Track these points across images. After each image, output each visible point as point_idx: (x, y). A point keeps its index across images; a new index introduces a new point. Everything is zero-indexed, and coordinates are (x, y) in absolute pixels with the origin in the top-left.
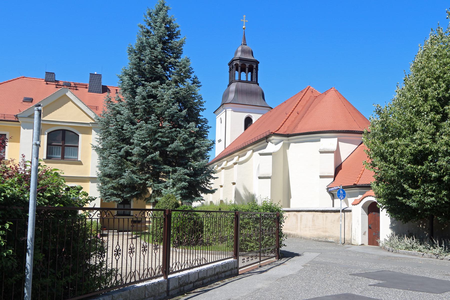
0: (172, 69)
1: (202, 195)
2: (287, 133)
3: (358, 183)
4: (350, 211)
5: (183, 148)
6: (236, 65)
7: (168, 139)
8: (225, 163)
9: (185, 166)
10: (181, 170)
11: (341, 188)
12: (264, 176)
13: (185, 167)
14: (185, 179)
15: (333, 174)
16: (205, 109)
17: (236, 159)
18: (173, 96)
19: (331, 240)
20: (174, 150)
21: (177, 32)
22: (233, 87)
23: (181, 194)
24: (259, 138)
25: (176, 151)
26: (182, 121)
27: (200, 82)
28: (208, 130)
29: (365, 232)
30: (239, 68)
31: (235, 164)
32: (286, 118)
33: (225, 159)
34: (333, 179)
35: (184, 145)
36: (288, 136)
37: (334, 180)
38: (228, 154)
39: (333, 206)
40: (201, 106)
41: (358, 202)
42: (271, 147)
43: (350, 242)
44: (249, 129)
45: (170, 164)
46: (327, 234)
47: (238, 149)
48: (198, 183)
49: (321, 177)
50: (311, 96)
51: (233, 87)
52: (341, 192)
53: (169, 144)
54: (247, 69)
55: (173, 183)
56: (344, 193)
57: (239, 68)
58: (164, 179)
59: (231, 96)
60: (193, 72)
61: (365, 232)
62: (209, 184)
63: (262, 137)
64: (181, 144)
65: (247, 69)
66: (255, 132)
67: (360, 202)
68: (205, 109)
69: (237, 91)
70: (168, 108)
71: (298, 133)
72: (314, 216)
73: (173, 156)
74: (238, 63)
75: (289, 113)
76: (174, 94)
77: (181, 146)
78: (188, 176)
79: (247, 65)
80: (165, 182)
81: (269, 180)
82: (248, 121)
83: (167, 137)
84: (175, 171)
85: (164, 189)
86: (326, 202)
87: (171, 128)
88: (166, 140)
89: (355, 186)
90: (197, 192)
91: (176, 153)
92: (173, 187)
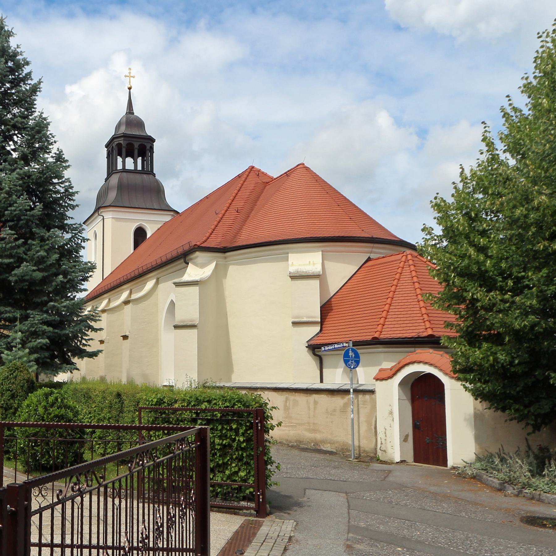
0: (18, 137)
1: (75, 360)
2: (223, 245)
3: (382, 336)
4: (372, 392)
5: (39, 275)
6: (119, 145)
7: (12, 260)
8: (105, 302)
9: (40, 306)
10: (36, 317)
11: (351, 345)
12: (185, 324)
13: (45, 309)
14: (44, 332)
15: (319, 320)
16: (77, 206)
17: (124, 295)
18: (21, 182)
19: (327, 447)
20: (21, 280)
21: (26, 75)
22: (115, 179)
23: (37, 361)
24: (169, 257)
25: (25, 281)
26: (37, 226)
27: (67, 161)
28: (83, 244)
29: (407, 436)
30: (124, 151)
31: (126, 302)
32: (218, 219)
33: (105, 296)
34: (317, 329)
35: (38, 270)
36: (224, 250)
37: (321, 330)
38: (110, 288)
39: (322, 381)
40: (70, 200)
41: (390, 375)
42: (193, 272)
43: (372, 455)
44: (143, 246)
45: (15, 305)
46: (318, 436)
47: (128, 277)
48: (67, 340)
49: (295, 324)
50: (257, 183)
51: (115, 179)
52: (350, 354)
53: (13, 269)
54: (136, 152)
55: (22, 340)
56: (357, 356)
57: (124, 151)
58: (5, 332)
59: (112, 195)
60: (55, 142)
61: (407, 436)
62: (86, 340)
63: (174, 254)
64: (35, 268)
65: (136, 152)
66: (151, 254)
67: (395, 374)
68: (77, 206)
69: (121, 187)
70: (11, 205)
71: (244, 243)
72: (287, 399)
73: (21, 290)
74: (122, 142)
75: (223, 212)
76: (22, 178)
77: (34, 271)
78: (48, 326)
79: (136, 145)
80: (8, 336)
81: (194, 332)
82: (140, 235)
83: (10, 256)
84: (25, 318)
85: (6, 352)
86: (306, 373)
87: (16, 240)
88: (7, 261)
89: (376, 342)
90: (65, 354)
91: (25, 285)
92: (24, 347)
